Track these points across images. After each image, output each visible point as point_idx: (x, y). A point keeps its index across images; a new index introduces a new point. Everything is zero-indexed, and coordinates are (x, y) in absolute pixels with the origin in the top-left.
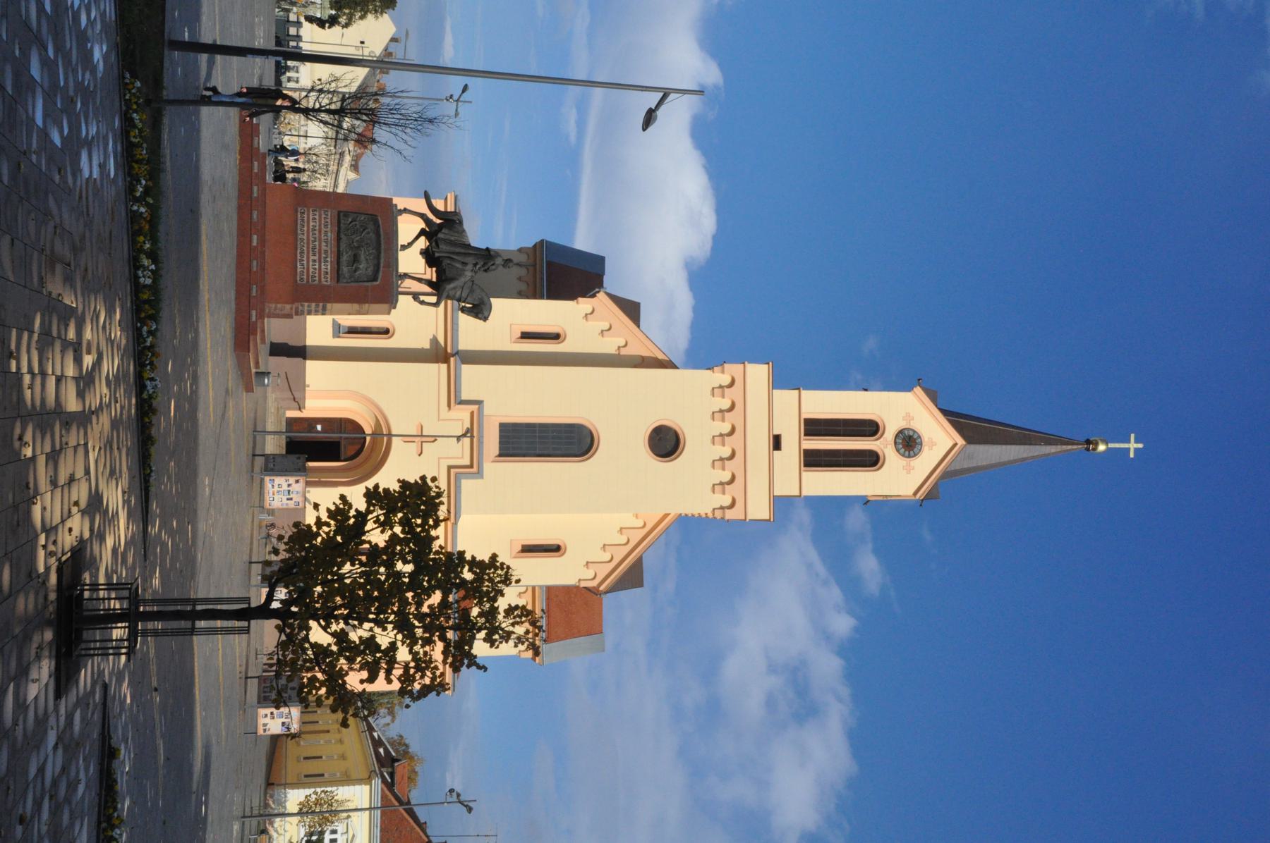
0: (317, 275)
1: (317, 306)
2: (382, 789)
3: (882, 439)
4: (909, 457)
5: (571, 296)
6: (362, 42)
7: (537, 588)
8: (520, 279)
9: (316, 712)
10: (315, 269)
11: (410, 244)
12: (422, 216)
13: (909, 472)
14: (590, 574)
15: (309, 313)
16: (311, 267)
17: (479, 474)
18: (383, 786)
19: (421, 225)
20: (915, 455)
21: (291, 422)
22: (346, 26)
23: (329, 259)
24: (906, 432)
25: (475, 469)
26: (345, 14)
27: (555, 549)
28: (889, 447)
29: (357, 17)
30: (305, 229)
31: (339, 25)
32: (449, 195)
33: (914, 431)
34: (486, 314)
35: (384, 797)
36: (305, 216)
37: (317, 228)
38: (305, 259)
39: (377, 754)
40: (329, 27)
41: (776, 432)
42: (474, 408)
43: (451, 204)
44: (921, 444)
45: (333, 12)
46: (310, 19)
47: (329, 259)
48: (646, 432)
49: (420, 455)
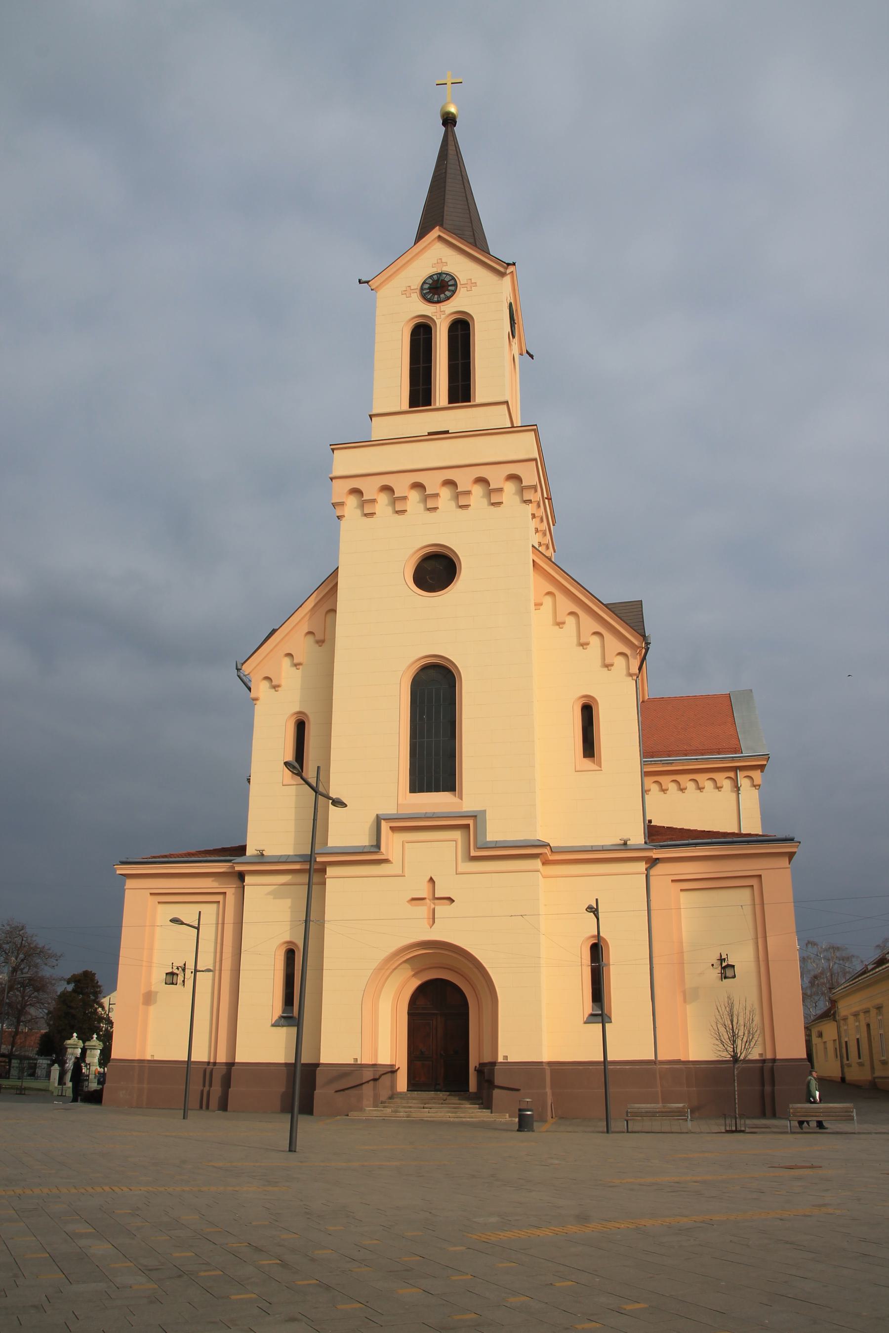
3: (434, 318)
4: (455, 285)
9: (846, 1042)
13: (404, 293)
14: (620, 662)
20: (453, 279)
21: (414, 1084)
25: (470, 822)
27: (588, 712)
28: (443, 308)
32: (118, 872)
33: (424, 283)
42: (385, 826)
43: (786, 847)
44: (440, 274)
49: (451, 900)
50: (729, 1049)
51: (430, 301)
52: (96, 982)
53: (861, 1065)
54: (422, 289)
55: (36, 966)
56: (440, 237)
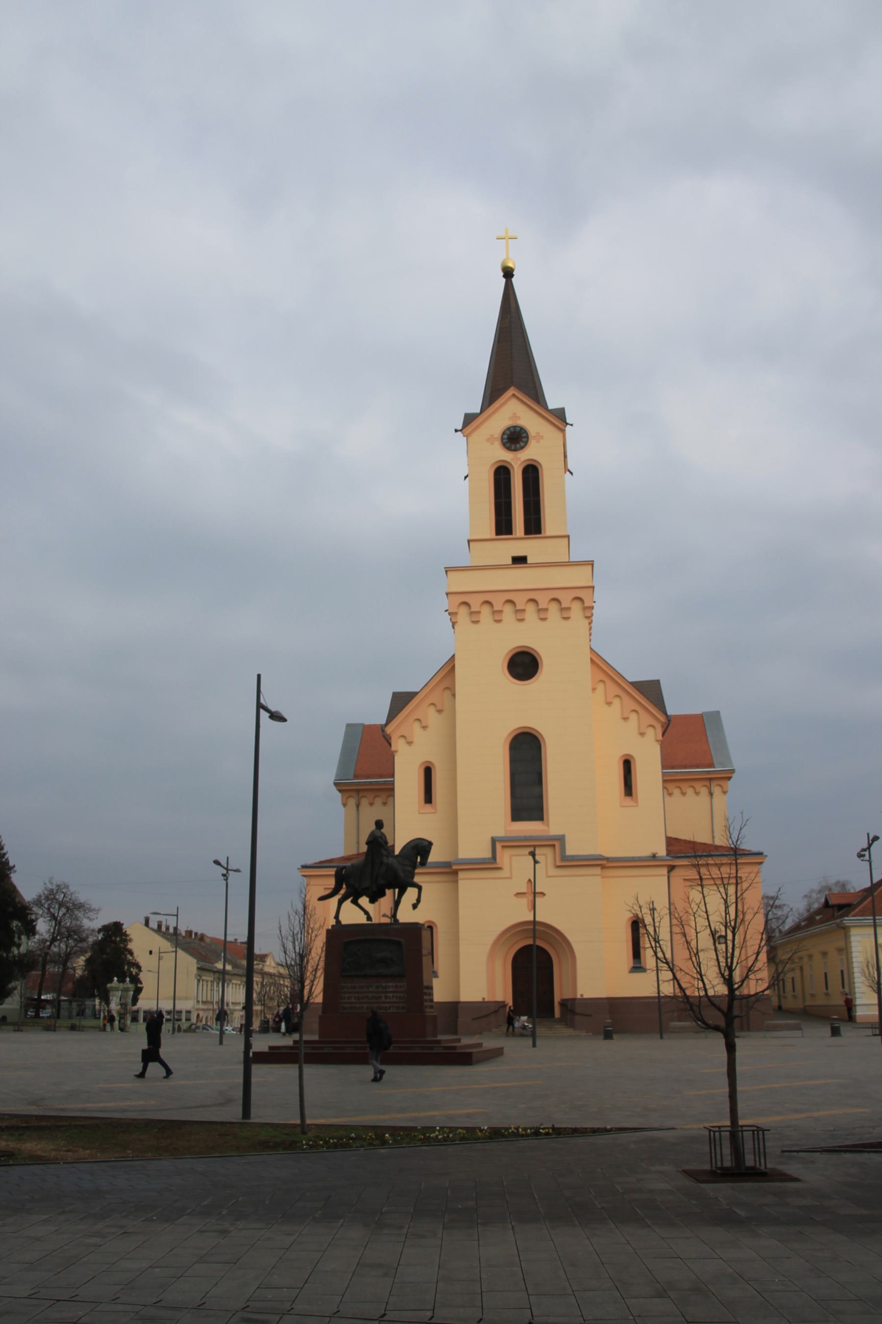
0: (398, 995)
1: (426, 994)
2: (853, 916)
3: (513, 463)
4: (527, 437)
5: (390, 758)
6: (151, 952)
7: (664, 778)
8: (371, 804)
10: (393, 996)
11: (366, 913)
12: (340, 903)
13: (488, 440)
15: (432, 1000)
16: (391, 1000)
17: (561, 839)
18: (850, 915)
19: (348, 904)
22: (139, 967)
23: (384, 984)
24: (504, 441)
26: (129, 969)
27: (627, 765)
29: (131, 958)
30: (358, 1006)
31: (139, 975)
33: (504, 433)
34: (426, 843)
35: (862, 913)
36: (346, 1006)
37: (357, 995)
38: (384, 1005)
39: (821, 922)
40: (141, 983)
41: (510, 562)
42: (498, 846)
45: (128, 979)
46: (135, 1000)
47: (384, 984)
48: (516, 684)
50: (695, 976)
51: (509, 449)
52: (124, 931)
53: (795, 997)
54: (502, 439)
55: (77, 919)
56: (514, 395)
